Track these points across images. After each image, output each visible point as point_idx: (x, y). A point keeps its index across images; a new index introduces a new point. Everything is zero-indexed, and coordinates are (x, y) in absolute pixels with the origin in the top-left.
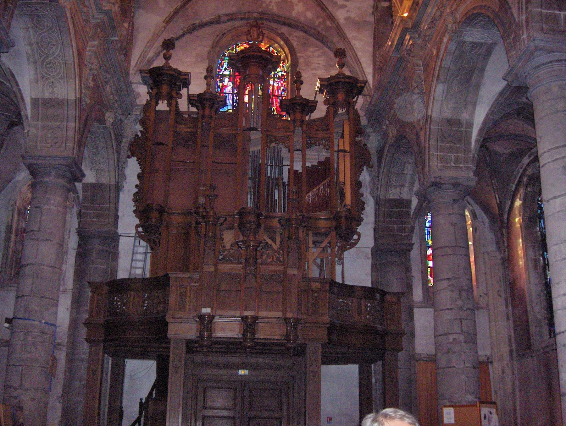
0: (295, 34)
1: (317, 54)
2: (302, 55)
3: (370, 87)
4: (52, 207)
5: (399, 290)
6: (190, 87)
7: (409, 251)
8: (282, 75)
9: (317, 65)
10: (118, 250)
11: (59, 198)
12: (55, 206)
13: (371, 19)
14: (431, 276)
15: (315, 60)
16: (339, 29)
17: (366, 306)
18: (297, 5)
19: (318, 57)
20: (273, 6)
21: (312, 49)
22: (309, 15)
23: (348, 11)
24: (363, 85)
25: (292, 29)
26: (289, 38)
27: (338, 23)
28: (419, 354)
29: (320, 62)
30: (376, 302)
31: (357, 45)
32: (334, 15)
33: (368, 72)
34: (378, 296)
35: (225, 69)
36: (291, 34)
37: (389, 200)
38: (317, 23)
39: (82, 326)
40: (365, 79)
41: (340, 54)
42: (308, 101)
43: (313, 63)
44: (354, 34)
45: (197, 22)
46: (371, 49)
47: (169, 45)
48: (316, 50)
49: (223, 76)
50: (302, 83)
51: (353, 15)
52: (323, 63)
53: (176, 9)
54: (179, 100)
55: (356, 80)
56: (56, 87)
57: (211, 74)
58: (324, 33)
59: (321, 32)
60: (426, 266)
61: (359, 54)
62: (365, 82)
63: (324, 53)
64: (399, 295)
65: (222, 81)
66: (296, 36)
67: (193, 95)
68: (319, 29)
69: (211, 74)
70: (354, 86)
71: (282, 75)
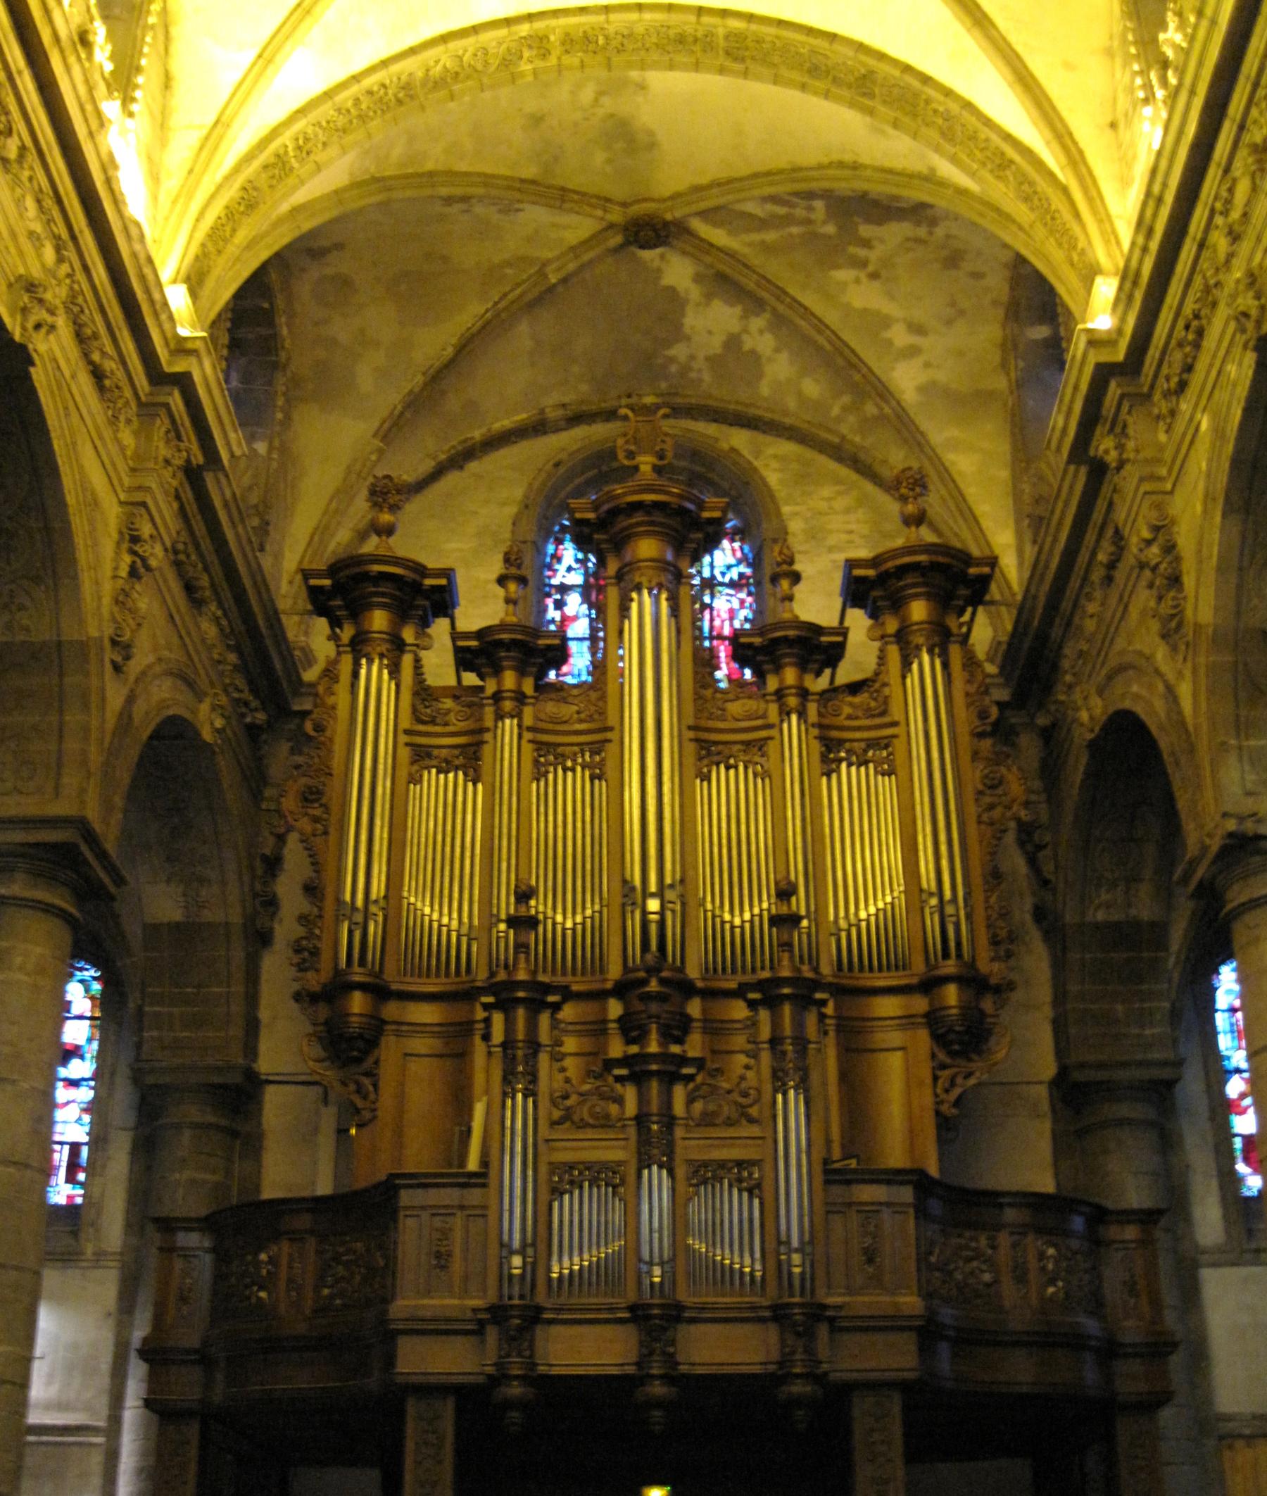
0: (771, 451)
1: (840, 503)
2: (797, 508)
3: (1010, 588)
4: (20, 976)
5: (1147, 1204)
6: (458, 612)
7: (1171, 1353)
8: (741, 575)
9: (844, 537)
10: (259, 1124)
11: (38, 950)
12: (28, 974)
13: (1001, 383)
14: (1247, 1160)
15: (836, 522)
16: (903, 425)
17: (1041, 1256)
18: (770, 359)
19: (847, 511)
20: (700, 371)
21: (826, 492)
22: (811, 388)
23: (927, 365)
24: (986, 570)
25: (761, 437)
26: (756, 463)
27: (899, 403)
28: (1229, 1418)
29: (853, 527)
30: (1075, 1244)
31: (963, 464)
32: (884, 379)
33: (1005, 544)
34: (1078, 1223)
35: (570, 569)
36: (758, 454)
37: (1097, 926)
38: (836, 411)
39: (133, 1356)
40: (987, 553)
41: (909, 486)
42: (817, 629)
43: (831, 532)
44: (953, 432)
45: (477, 434)
46: (1004, 474)
47: (387, 495)
48: (839, 493)
49: (564, 589)
50: (796, 578)
51: (941, 376)
52: (865, 529)
53: (411, 392)
54: (423, 654)
55: (965, 558)
56: (22, 608)
57: (523, 573)
58: (857, 439)
59: (849, 437)
60: (1226, 1134)
61: (972, 492)
62: (993, 562)
63: (863, 501)
64: (1147, 1218)
65: (559, 605)
66: (775, 456)
67: (467, 636)
68: (844, 429)
69: (523, 573)
70: (955, 578)
71: (741, 575)
